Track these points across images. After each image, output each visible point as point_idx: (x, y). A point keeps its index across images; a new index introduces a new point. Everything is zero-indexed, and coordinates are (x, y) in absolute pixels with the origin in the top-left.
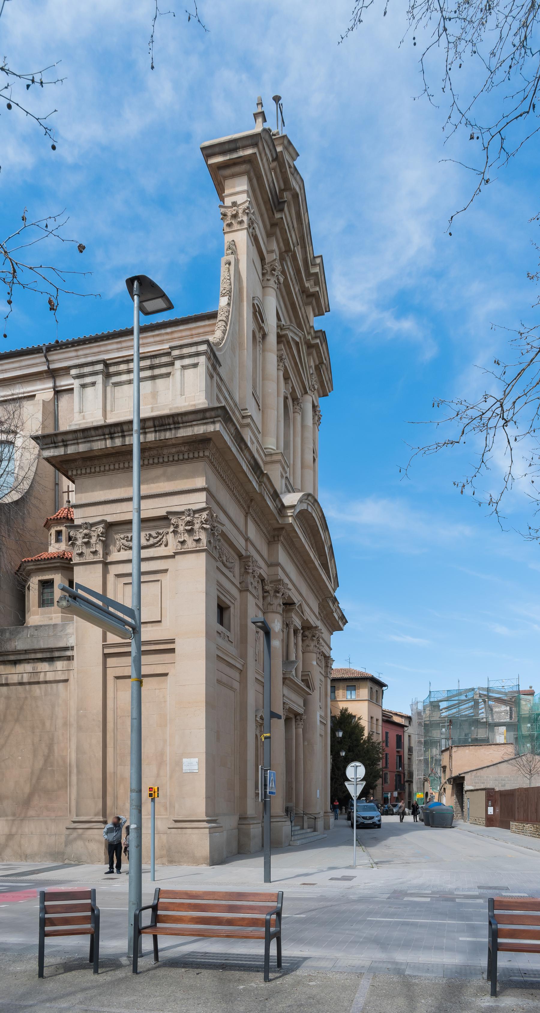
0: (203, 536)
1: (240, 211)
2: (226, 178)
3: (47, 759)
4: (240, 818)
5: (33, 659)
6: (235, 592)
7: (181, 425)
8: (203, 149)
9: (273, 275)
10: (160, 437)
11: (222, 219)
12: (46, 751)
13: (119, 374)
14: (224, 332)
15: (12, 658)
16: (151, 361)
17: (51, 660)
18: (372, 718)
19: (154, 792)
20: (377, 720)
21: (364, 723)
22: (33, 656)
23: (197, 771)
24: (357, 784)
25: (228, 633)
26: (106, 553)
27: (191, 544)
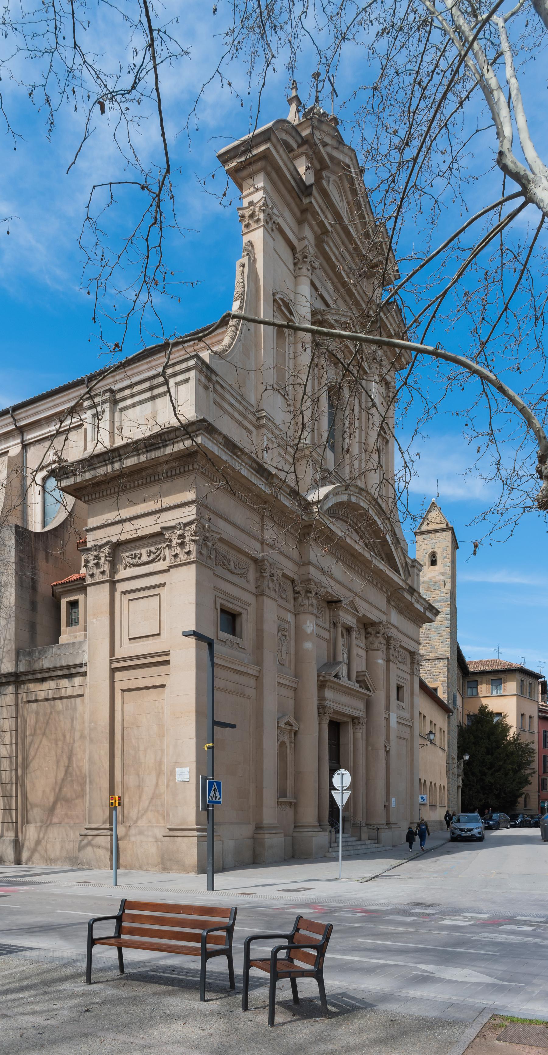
0: (192, 548)
1: (257, 209)
2: (244, 179)
3: (67, 771)
4: (256, 828)
5: (56, 676)
6: (250, 599)
7: (168, 442)
8: (219, 157)
9: (305, 262)
10: (151, 456)
11: (240, 221)
12: (67, 762)
13: (124, 399)
14: (233, 338)
15: (39, 676)
16: (150, 383)
17: (70, 676)
18: (522, 715)
19: (116, 801)
20: (531, 717)
21: (512, 720)
22: (55, 673)
23: (188, 780)
24: (343, 793)
25: (239, 640)
26: (114, 571)
27: (183, 557)
